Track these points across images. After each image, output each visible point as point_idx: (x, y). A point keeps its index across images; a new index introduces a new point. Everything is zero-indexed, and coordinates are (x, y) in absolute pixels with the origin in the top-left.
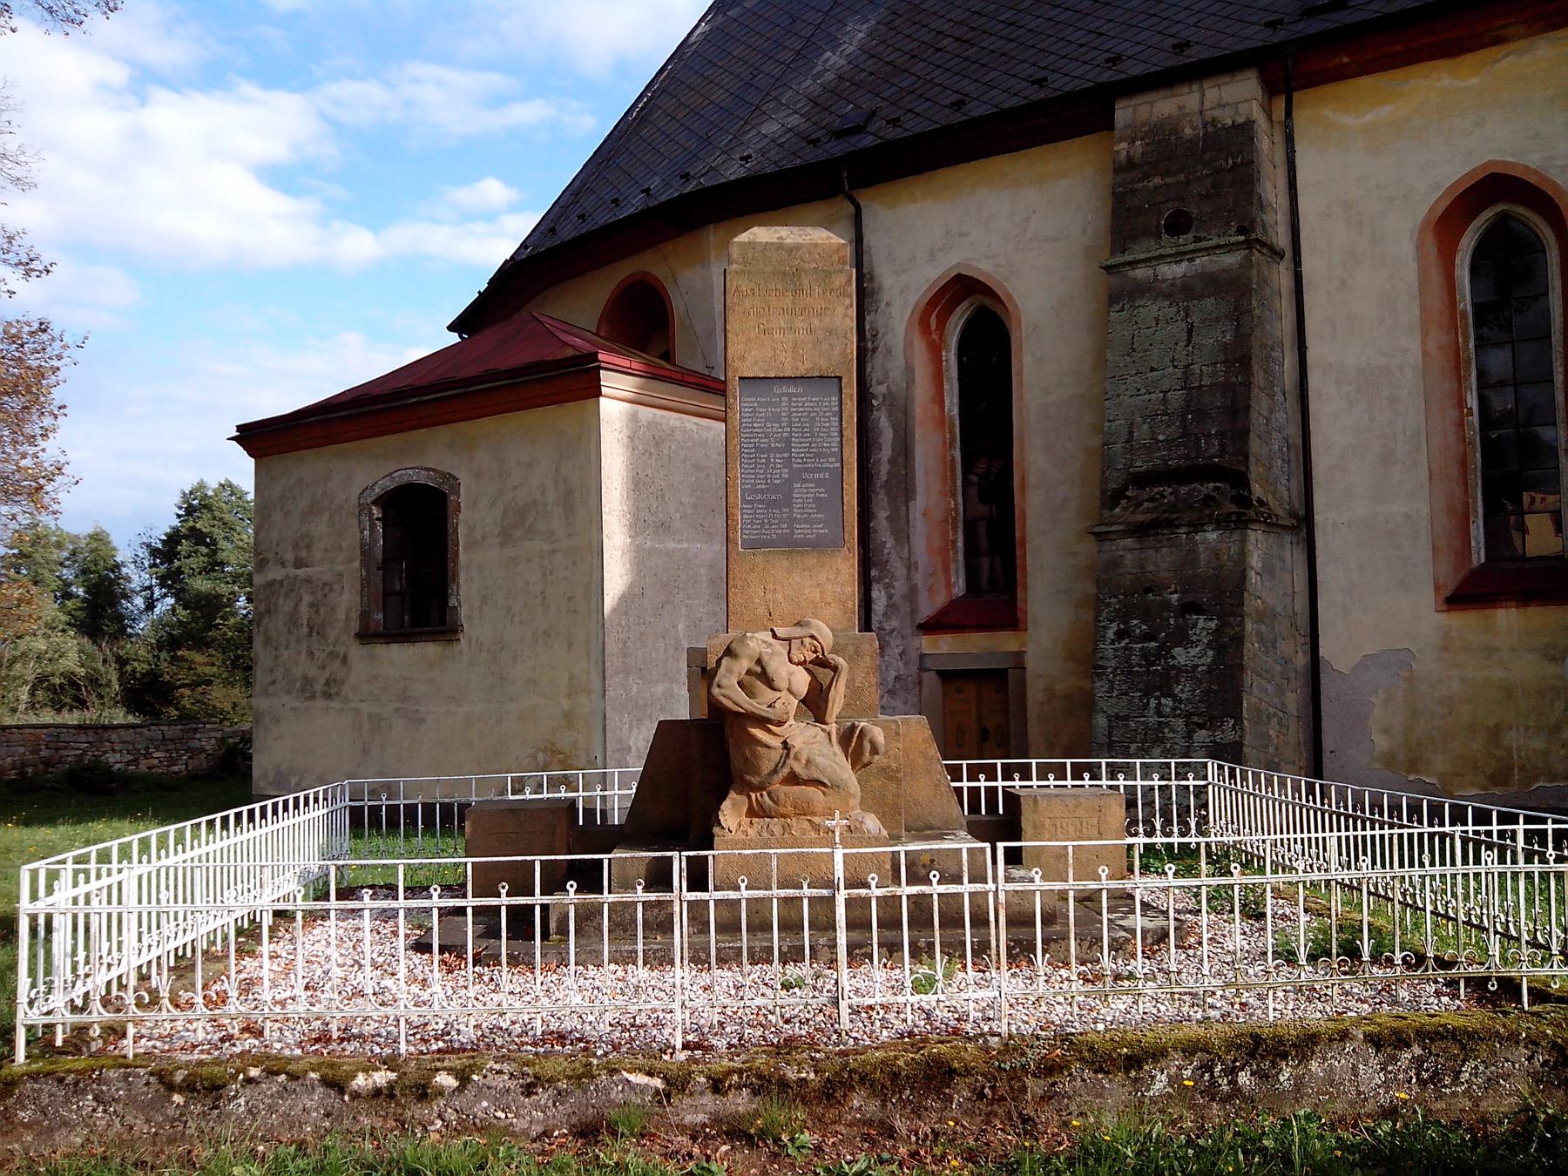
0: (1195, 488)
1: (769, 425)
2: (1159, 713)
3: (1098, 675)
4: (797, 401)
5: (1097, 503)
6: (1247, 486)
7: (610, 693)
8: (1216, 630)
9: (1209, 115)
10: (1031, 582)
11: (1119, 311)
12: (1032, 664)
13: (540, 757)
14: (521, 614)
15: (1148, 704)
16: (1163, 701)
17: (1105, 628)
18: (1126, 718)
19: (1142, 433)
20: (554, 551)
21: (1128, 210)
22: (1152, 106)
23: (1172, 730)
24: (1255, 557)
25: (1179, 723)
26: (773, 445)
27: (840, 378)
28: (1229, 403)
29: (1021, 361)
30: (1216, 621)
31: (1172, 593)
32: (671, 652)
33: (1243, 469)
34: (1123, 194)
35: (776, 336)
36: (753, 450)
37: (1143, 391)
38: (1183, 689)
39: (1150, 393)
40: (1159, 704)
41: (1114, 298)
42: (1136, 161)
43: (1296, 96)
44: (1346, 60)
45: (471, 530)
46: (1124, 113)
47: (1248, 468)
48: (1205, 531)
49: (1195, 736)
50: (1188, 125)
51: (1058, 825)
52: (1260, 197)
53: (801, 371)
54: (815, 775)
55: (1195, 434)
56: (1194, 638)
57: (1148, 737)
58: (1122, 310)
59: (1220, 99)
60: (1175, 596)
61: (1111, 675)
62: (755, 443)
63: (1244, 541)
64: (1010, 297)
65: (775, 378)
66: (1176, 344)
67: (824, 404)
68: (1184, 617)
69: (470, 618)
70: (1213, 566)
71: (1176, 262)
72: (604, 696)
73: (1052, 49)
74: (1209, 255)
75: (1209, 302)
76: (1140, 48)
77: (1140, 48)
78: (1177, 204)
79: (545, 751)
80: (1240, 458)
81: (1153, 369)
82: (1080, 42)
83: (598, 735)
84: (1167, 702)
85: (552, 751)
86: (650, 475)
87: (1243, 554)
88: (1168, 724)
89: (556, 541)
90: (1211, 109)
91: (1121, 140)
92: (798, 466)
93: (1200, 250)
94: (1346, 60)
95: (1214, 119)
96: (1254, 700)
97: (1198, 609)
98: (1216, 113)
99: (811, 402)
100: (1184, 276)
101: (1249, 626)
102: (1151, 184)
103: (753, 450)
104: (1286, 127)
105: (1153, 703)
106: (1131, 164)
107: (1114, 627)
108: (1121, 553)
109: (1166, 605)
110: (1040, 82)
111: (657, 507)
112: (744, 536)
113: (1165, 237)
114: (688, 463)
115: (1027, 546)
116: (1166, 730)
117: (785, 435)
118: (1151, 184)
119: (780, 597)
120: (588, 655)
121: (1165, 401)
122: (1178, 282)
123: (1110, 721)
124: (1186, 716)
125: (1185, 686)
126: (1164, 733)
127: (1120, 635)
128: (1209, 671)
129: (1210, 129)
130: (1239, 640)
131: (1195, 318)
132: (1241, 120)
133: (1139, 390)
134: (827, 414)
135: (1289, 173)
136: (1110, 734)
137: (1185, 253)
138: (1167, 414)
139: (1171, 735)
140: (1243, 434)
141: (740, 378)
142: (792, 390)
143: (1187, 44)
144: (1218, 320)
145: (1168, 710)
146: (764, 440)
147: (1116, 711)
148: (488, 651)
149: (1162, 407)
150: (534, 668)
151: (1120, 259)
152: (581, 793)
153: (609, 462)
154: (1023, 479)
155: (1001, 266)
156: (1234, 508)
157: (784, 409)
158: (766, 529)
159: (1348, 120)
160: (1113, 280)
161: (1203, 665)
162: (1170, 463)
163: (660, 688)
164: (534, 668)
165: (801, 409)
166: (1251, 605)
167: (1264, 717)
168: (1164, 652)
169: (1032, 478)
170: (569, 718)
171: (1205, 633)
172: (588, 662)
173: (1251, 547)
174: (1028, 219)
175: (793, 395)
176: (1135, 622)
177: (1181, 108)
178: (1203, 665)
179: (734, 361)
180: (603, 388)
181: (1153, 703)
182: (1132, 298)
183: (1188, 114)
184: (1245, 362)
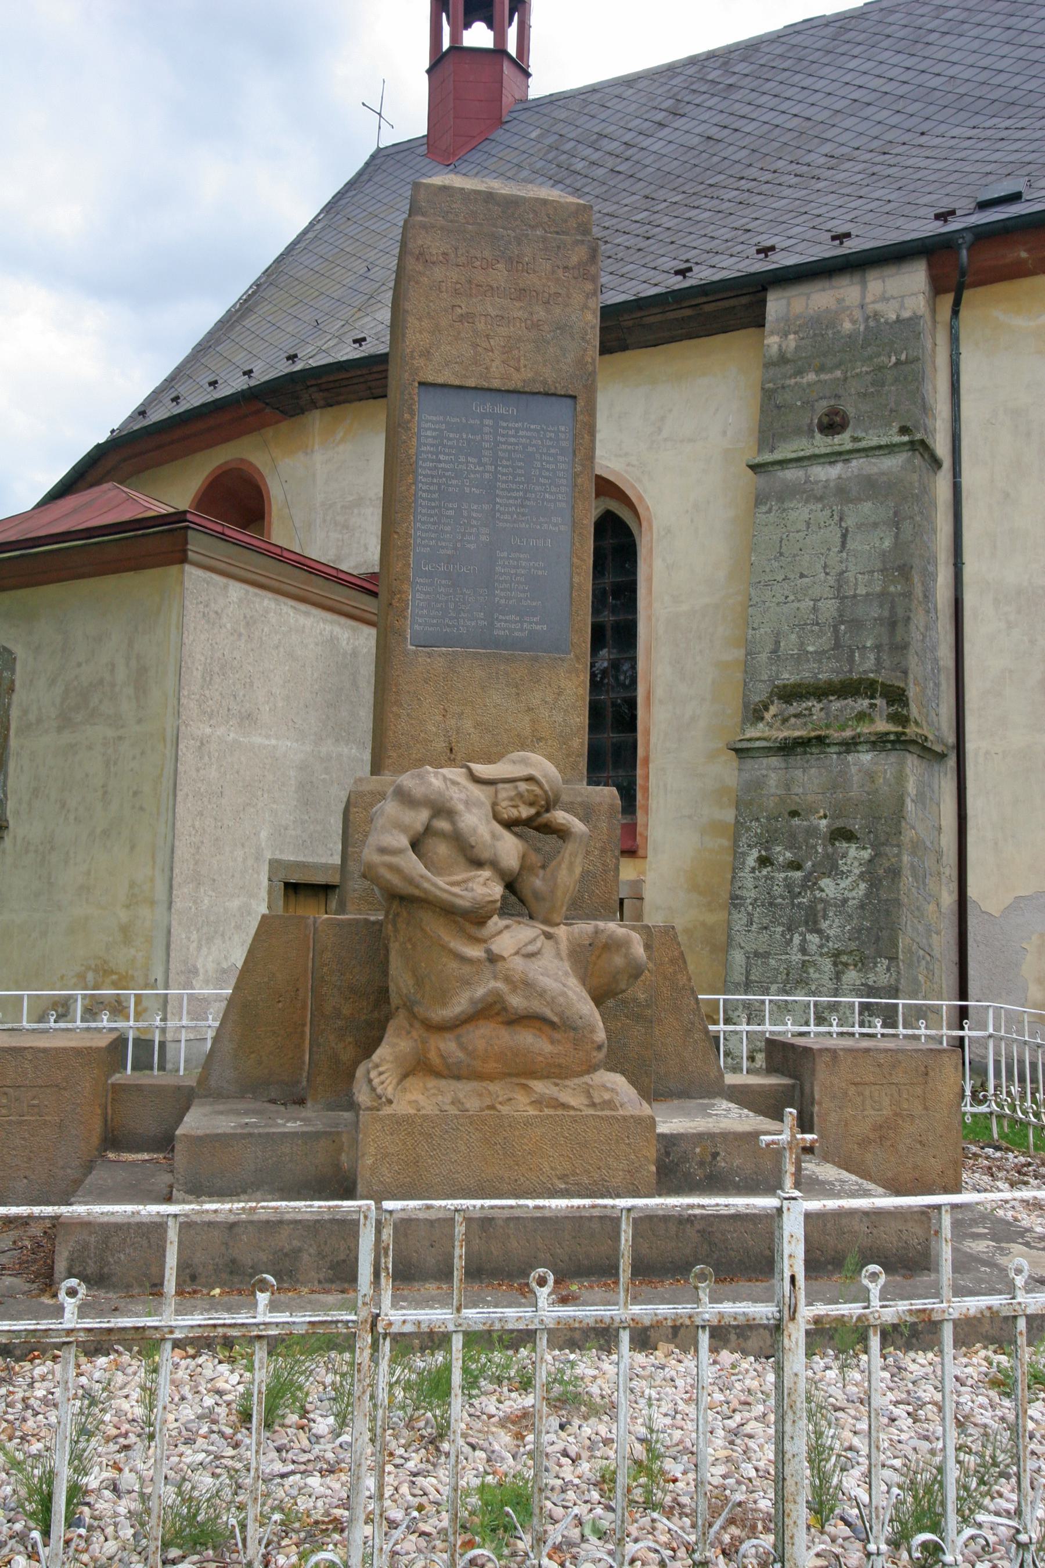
0: (847, 705)
1: (462, 459)
2: (803, 951)
3: (735, 906)
4: (508, 428)
5: (738, 719)
6: (906, 704)
7: (178, 904)
8: (870, 861)
9: (870, 308)
10: (653, 804)
11: (766, 513)
12: (648, 894)
13: (90, 976)
14: (76, 809)
15: (791, 940)
16: (809, 937)
17: (744, 854)
18: (766, 955)
19: (790, 643)
20: (120, 738)
21: (778, 407)
22: (808, 299)
23: (818, 970)
24: (911, 782)
25: (827, 964)
26: (467, 490)
27: (574, 397)
28: (886, 614)
29: (650, 566)
30: (869, 851)
31: (820, 818)
32: (250, 862)
33: (902, 685)
34: (774, 391)
35: (481, 326)
36: (436, 496)
37: (791, 598)
38: (832, 926)
39: (799, 601)
40: (804, 940)
41: (760, 499)
42: (789, 356)
43: (967, 294)
44: (1024, 255)
45: (25, 712)
46: (776, 305)
47: (907, 684)
48: (858, 752)
49: (845, 978)
50: (847, 319)
51: (867, 1093)
52: (923, 399)
53: (516, 381)
54: (537, 1006)
55: (849, 647)
56: (845, 869)
57: (791, 977)
58: (770, 511)
59: (884, 292)
60: (824, 822)
61: (750, 907)
62: (439, 485)
63: (902, 764)
64: (641, 498)
65: (475, 388)
66: (829, 549)
67: (549, 435)
68: (833, 845)
69: (17, 813)
70: (866, 789)
71: (831, 463)
72: (170, 908)
73: (694, 244)
74: (867, 456)
75: (867, 507)
76: (792, 241)
77: (792, 241)
78: (832, 403)
79: (96, 971)
80: (899, 674)
81: (802, 576)
82: (724, 238)
83: (160, 953)
84: (814, 939)
85: (105, 971)
86: (238, 658)
87: (900, 778)
88: (814, 964)
89: (122, 727)
90: (873, 302)
91: (772, 333)
92: (505, 525)
93: (858, 451)
94: (1024, 255)
95: (876, 315)
96: (908, 940)
97: (848, 835)
98: (879, 307)
99: (528, 430)
100: (839, 478)
101: (906, 858)
102: (805, 381)
103: (436, 496)
104: (952, 327)
105: (797, 939)
106: (783, 359)
107: (755, 854)
108: (764, 772)
109: (812, 832)
110: (682, 273)
111: (244, 696)
112: (416, 627)
113: (818, 435)
114: (282, 650)
115: (651, 766)
116: (811, 970)
117: (487, 476)
118: (805, 381)
119: (468, 724)
120: (153, 857)
121: (815, 609)
122: (832, 484)
123: (748, 958)
124: (834, 955)
125: (833, 921)
126: (808, 974)
127: (764, 861)
128: (862, 906)
129: (872, 324)
130: (895, 873)
131: (850, 522)
132: (906, 314)
133: (787, 597)
134: (553, 451)
135: (952, 376)
136: (748, 973)
137: (840, 453)
138: (818, 624)
139: (817, 975)
140: (900, 648)
141: (421, 384)
142: (500, 410)
143: (848, 235)
144: (875, 525)
145: (815, 948)
146: (454, 482)
147: (754, 946)
148: (36, 851)
149: (812, 616)
150: (89, 873)
151: (767, 457)
152: (131, 1023)
153: (191, 638)
154: (649, 693)
155: (633, 466)
156: (891, 727)
157: (486, 437)
158: (451, 619)
159: (1019, 322)
160: (760, 481)
161: (854, 899)
162: (820, 676)
163: (235, 904)
164: (89, 873)
165: (513, 440)
166: (908, 835)
167: (915, 959)
168: (810, 883)
169: (659, 692)
170: (126, 932)
171: (856, 864)
172: (153, 868)
173: (908, 771)
174: (663, 419)
175: (502, 417)
176: (778, 849)
177: (840, 301)
178: (854, 899)
179: (413, 358)
180: (190, 553)
181: (797, 939)
182: (781, 499)
183: (848, 307)
184: (904, 572)
